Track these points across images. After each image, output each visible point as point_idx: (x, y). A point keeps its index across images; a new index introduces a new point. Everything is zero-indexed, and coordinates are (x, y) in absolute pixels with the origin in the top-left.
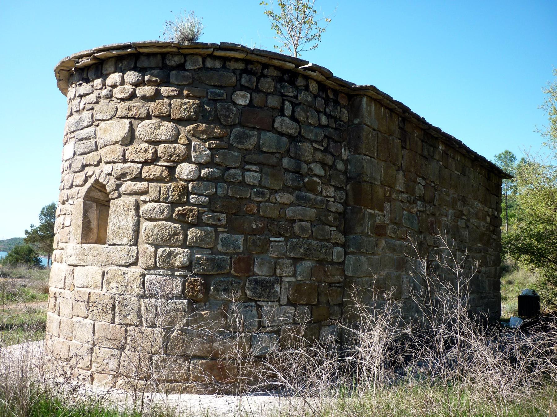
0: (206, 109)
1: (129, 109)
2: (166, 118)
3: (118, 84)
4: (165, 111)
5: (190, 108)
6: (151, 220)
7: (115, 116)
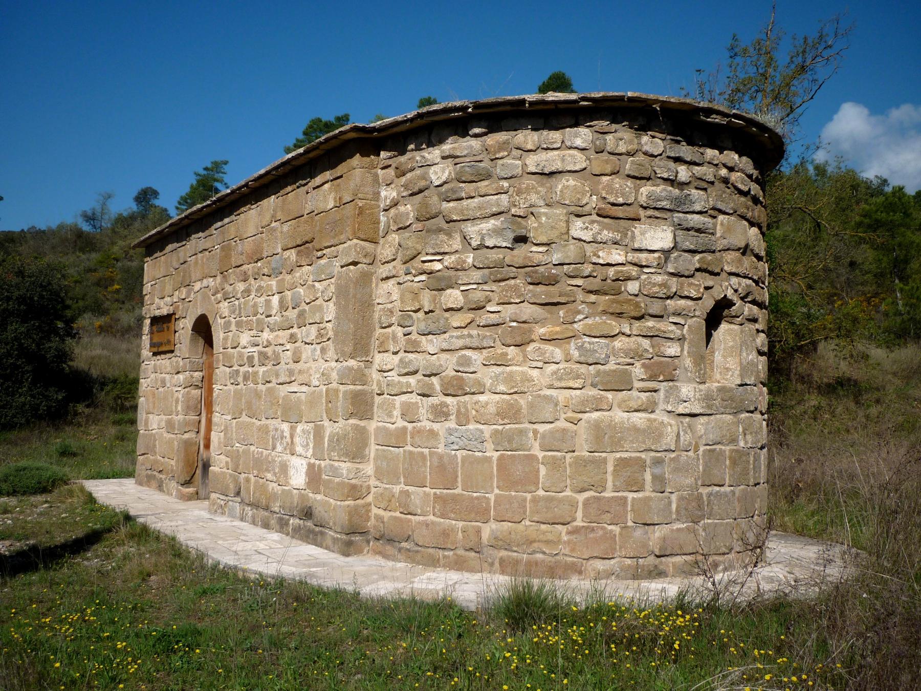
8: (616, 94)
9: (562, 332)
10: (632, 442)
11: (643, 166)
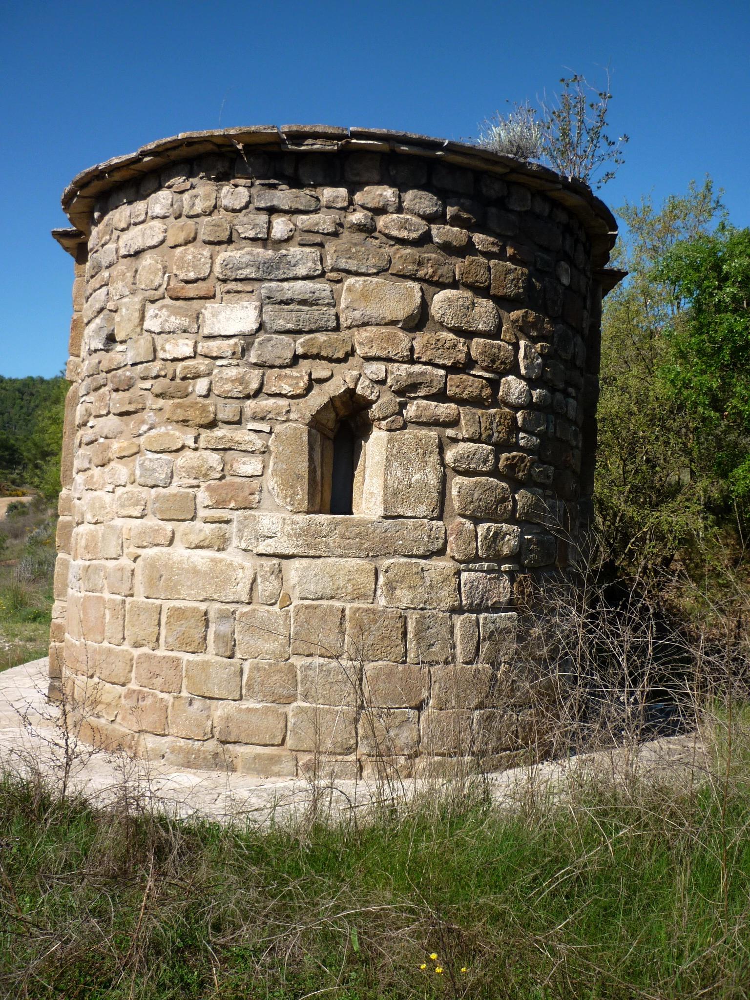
0: (535, 286)
1: (420, 264)
2: (482, 291)
3: (391, 209)
4: (484, 279)
5: (518, 279)
6: (467, 473)
7: (387, 270)
8: (169, 139)
9: (128, 448)
10: (190, 587)
11: (219, 226)
